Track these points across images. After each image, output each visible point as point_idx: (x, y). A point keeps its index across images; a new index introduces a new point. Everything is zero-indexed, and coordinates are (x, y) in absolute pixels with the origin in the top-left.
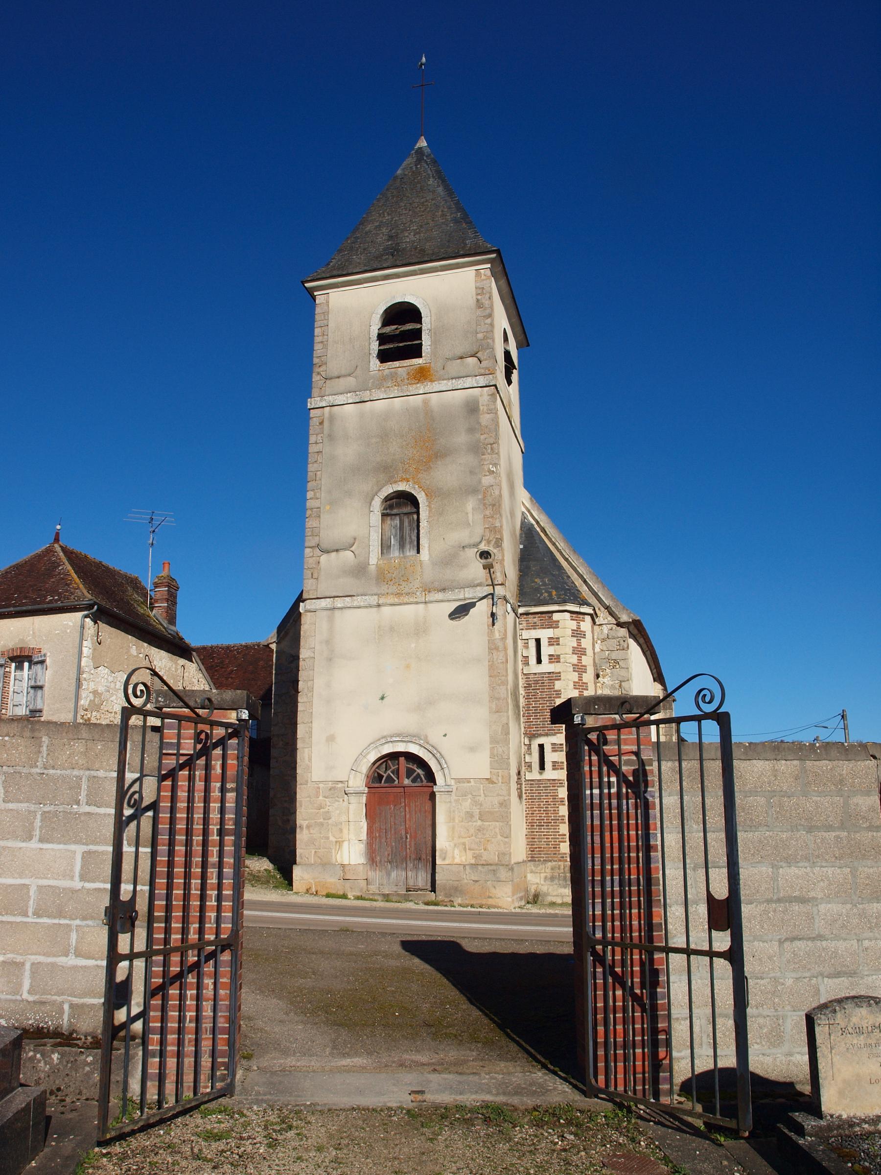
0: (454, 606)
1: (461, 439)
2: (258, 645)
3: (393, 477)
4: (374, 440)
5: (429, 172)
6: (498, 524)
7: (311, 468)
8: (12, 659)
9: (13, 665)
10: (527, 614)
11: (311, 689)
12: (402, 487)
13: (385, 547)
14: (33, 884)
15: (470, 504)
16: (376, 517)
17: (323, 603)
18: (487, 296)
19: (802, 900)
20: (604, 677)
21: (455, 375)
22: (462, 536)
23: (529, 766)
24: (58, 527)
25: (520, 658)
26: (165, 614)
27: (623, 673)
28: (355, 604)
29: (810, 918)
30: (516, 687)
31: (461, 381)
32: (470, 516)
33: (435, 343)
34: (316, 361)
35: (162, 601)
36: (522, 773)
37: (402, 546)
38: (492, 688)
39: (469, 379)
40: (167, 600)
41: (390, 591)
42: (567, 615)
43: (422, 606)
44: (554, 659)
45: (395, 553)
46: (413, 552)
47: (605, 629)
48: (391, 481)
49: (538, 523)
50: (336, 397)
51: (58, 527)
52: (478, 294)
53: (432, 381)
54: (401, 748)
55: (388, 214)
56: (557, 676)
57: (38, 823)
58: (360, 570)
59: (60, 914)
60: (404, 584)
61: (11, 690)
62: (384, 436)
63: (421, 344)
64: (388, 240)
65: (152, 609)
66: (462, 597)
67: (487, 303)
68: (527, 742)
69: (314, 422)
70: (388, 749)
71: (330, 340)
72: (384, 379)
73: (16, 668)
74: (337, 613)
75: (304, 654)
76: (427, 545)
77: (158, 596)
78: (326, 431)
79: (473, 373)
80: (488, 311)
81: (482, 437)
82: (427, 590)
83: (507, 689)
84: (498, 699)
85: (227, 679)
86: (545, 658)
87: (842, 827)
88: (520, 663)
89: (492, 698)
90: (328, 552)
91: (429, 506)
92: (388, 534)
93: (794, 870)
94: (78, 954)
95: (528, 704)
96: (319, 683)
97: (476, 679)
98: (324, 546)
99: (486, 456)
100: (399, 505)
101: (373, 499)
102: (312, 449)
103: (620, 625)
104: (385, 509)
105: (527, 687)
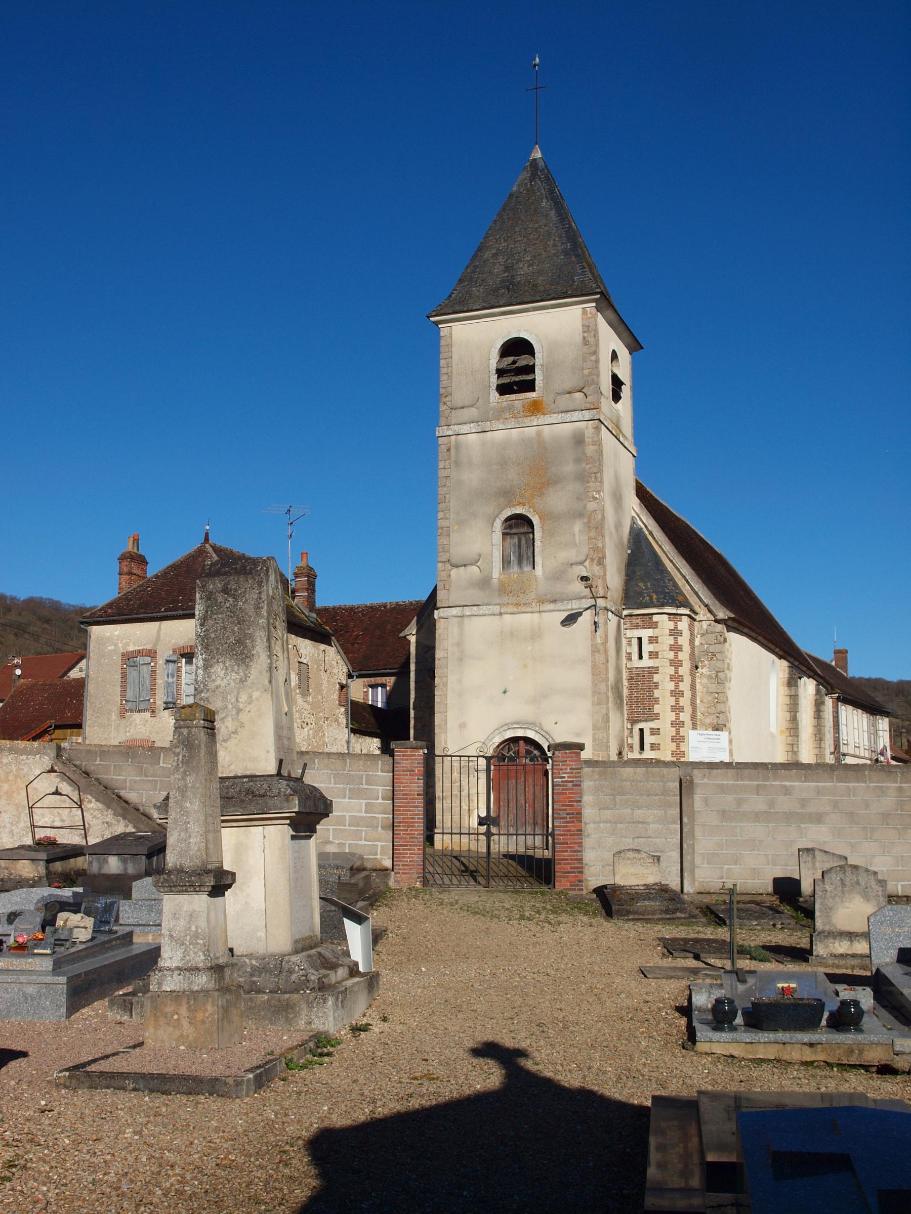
0: (565, 615)
1: (569, 468)
2: (385, 606)
3: (511, 501)
4: (495, 467)
5: (543, 192)
6: (600, 545)
7: (441, 491)
8: (183, 656)
9: (184, 660)
10: (631, 615)
11: (445, 684)
12: (519, 510)
13: (506, 563)
14: (347, 815)
15: (578, 526)
16: (498, 536)
17: (454, 611)
18: (593, 333)
19: (643, 823)
20: (703, 667)
21: (563, 408)
22: (571, 555)
23: (631, 747)
24: (208, 527)
25: (624, 654)
26: (306, 603)
27: (719, 664)
28: (481, 612)
29: (646, 830)
30: (618, 680)
31: (569, 414)
32: (577, 536)
33: (547, 378)
34: (442, 391)
35: (302, 590)
36: (624, 753)
37: (520, 562)
38: (595, 685)
39: (576, 413)
40: (307, 589)
41: (510, 602)
42: (666, 616)
43: (537, 615)
44: (653, 655)
45: (515, 569)
46: (529, 568)
47: (705, 625)
48: (510, 505)
49: (646, 526)
50: (460, 426)
51: (208, 527)
52: (584, 332)
53: (544, 414)
54: (520, 733)
55: (505, 240)
56: (654, 670)
57: (347, 792)
58: (484, 583)
59: (358, 826)
60: (522, 595)
61: (183, 682)
62: (503, 464)
63: (534, 380)
64: (505, 272)
65: (293, 598)
66: (570, 607)
67: (592, 340)
68: (629, 727)
69: (443, 449)
70: (509, 734)
71: (454, 372)
72: (503, 410)
73: (186, 663)
74: (466, 620)
75: (439, 654)
76: (540, 562)
77: (299, 586)
78: (453, 459)
79: (580, 408)
80: (593, 348)
81: (588, 467)
82: (541, 601)
83: (607, 686)
84: (599, 694)
85: (353, 644)
86: (645, 655)
87: (662, 795)
88: (624, 658)
89: (595, 693)
90: (457, 566)
91: (542, 528)
92: (508, 550)
93: (640, 811)
94: (365, 840)
95: (631, 695)
96: (452, 679)
97: (581, 677)
98: (453, 561)
99: (591, 484)
100: (517, 526)
101: (494, 520)
102: (442, 473)
103: (717, 621)
104: (506, 528)
105: (630, 679)
